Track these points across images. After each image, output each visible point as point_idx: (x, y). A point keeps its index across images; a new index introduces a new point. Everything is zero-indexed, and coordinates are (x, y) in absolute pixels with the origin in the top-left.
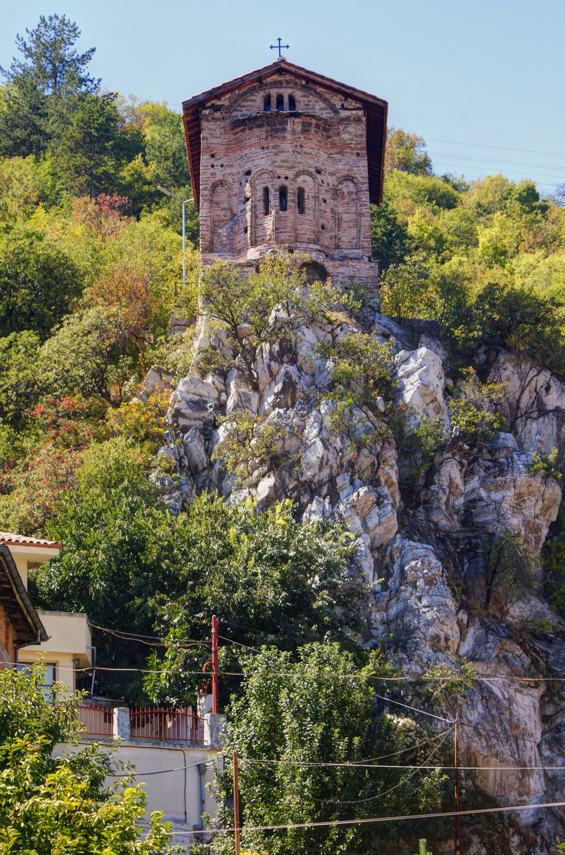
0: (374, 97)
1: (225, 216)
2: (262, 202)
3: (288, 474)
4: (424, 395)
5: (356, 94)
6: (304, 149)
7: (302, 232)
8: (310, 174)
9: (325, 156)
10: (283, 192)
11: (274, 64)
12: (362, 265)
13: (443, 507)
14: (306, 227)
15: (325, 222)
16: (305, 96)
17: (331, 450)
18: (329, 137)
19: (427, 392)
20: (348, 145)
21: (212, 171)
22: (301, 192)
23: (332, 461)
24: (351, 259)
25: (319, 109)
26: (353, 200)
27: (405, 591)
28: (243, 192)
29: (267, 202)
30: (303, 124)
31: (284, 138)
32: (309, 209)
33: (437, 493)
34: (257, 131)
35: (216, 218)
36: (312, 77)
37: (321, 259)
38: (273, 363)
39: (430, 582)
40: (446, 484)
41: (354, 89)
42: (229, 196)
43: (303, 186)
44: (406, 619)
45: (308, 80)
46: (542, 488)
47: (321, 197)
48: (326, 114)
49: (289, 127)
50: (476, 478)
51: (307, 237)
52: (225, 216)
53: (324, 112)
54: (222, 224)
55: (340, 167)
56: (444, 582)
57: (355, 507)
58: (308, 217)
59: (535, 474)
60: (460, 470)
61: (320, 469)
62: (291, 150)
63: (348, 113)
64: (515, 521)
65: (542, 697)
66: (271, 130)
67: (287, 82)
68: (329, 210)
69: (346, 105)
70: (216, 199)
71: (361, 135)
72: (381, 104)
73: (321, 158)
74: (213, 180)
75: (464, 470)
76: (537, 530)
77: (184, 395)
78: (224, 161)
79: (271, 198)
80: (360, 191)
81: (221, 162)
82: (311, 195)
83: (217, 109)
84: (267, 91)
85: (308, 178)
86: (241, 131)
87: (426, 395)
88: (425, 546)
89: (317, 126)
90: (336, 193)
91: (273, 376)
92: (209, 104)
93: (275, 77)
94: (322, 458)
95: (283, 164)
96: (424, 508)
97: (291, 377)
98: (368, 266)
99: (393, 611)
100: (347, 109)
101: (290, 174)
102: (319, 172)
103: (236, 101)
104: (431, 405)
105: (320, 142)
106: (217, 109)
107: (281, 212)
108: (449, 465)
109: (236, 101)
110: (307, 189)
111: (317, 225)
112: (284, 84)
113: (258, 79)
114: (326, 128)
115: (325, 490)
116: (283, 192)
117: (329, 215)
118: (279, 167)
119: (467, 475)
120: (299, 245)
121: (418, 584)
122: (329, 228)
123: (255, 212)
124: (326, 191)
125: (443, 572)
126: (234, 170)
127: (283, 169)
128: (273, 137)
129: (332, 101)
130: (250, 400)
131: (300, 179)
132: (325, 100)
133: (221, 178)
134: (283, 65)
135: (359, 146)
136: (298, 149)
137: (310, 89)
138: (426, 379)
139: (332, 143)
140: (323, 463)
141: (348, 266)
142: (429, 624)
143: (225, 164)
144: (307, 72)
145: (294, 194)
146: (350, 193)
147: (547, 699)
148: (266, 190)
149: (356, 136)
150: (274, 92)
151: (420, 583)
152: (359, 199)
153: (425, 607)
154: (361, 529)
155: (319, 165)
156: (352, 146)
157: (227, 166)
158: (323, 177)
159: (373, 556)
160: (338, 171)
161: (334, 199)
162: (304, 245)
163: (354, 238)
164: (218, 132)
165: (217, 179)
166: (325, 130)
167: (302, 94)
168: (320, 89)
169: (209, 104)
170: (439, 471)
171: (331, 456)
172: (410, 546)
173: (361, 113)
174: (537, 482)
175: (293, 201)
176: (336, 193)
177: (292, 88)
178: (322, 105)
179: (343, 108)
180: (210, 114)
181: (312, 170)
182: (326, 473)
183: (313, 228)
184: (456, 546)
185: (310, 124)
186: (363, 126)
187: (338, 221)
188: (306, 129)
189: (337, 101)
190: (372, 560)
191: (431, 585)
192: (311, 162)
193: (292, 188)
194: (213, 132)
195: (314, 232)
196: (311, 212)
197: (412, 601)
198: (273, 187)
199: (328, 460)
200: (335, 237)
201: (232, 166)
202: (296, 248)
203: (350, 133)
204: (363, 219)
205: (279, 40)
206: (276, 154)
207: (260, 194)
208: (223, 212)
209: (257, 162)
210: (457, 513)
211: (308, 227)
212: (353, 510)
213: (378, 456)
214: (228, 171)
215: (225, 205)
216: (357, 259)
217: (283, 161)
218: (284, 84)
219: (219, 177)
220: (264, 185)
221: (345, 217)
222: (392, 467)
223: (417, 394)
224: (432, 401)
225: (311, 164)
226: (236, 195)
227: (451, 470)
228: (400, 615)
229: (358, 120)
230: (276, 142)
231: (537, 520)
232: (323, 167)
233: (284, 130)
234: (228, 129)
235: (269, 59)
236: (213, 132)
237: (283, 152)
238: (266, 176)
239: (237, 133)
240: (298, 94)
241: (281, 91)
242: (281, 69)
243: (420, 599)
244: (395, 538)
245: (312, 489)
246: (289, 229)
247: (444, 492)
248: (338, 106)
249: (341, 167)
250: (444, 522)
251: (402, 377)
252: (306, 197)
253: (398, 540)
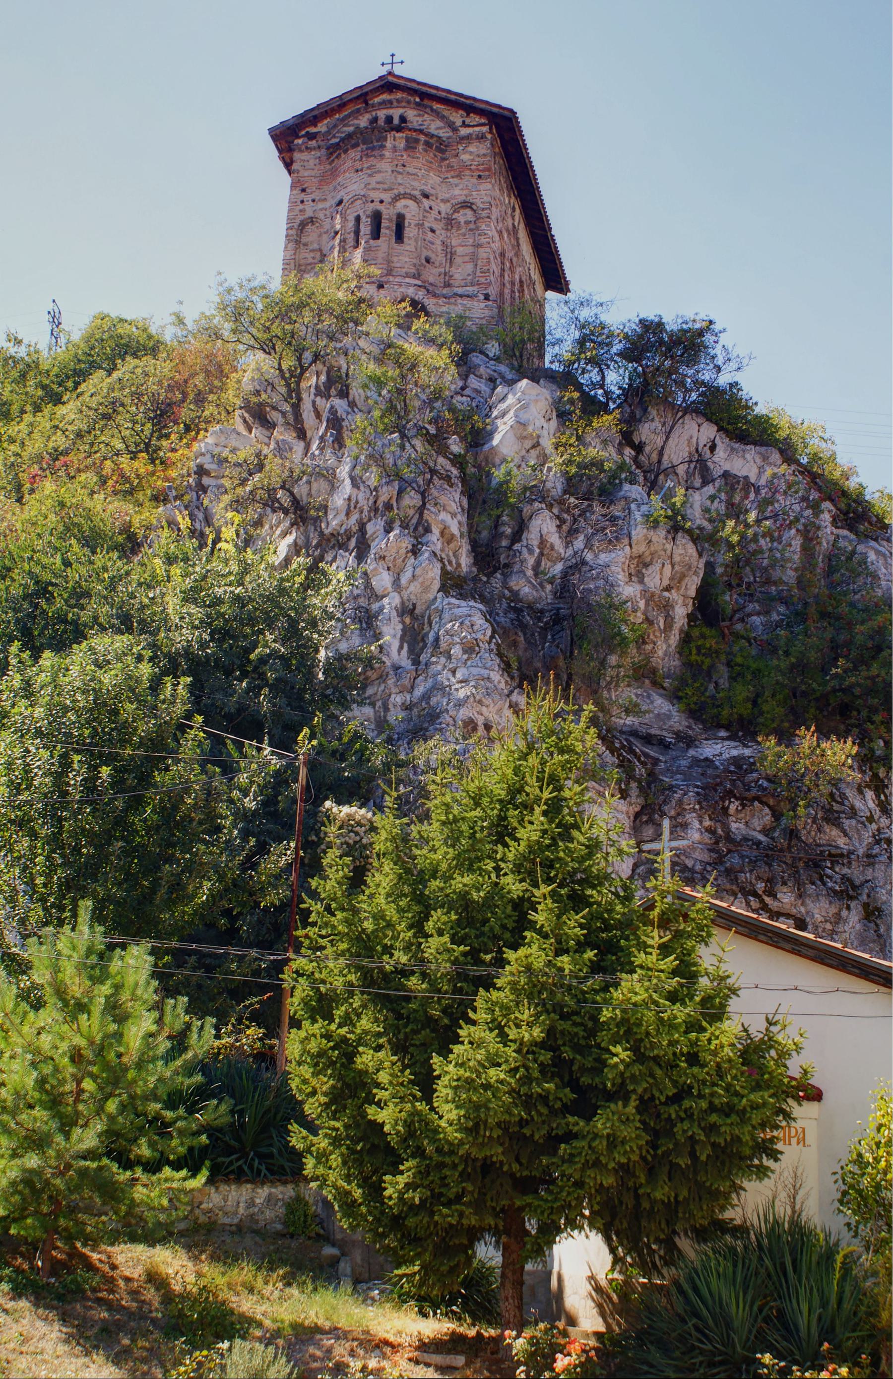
0: (499, 107)
4: (522, 438)
5: (477, 105)
8: (413, 198)
9: (438, 180)
10: (377, 218)
13: (530, 573)
20: (468, 167)
21: (301, 207)
23: (362, 502)
24: (461, 296)
25: (435, 126)
28: (333, 227)
29: (357, 232)
30: (407, 139)
31: (382, 156)
34: (352, 153)
36: (424, 89)
37: (420, 295)
38: (318, 399)
39: (470, 649)
40: (535, 543)
41: (474, 99)
42: (320, 236)
44: (434, 701)
45: (424, 95)
46: (668, 547)
47: (427, 225)
49: (389, 144)
50: (581, 537)
55: (457, 192)
57: (383, 558)
59: (655, 525)
61: (348, 514)
64: (629, 591)
65: (637, 815)
67: (398, 101)
68: (438, 242)
69: (468, 121)
70: (304, 240)
72: (506, 113)
73: (432, 181)
75: (565, 528)
76: (666, 607)
78: (316, 195)
81: (313, 196)
82: (413, 223)
83: (312, 137)
85: (410, 203)
88: (472, 603)
89: (427, 144)
90: (450, 223)
93: (385, 97)
94: (349, 499)
98: (482, 305)
99: (419, 691)
102: (427, 196)
103: (335, 126)
106: (312, 137)
108: (541, 517)
109: (335, 126)
110: (408, 216)
111: (419, 257)
113: (362, 97)
114: (440, 148)
115: (353, 543)
116: (377, 218)
117: (439, 248)
119: (570, 535)
125: (492, 637)
126: (327, 205)
128: (368, 156)
134: (390, 78)
136: (400, 168)
137: (426, 107)
138: (524, 417)
139: (449, 166)
142: (460, 704)
144: (419, 83)
145: (390, 220)
146: (467, 223)
147: (645, 818)
148: (358, 219)
150: (382, 114)
151: (456, 651)
152: (477, 228)
155: (428, 189)
159: (403, 622)
160: (454, 197)
162: (398, 279)
167: (415, 112)
168: (436, 106)
171: (361, 496)
173: (485, 129)
174: (659, 536)
175: (388, 228)
176: (450, 223)
178: (439, 123)
179: (464, 125)
182: (354, 517)
184: (540, 619)
185: (417, 141)
187: (450, 255)
188: (411, 145)
189: (457, 117)
190: (400, 626)
192: (416, 184)
193: (389, 213)
196: (412, 242)
197: (445, 677)
198: (364, 211)
202: (387, 282)
204: (481, 250)
207: (351, 224)
209: (350, 189)
210: (551, 581)
212: (381, 563)
213: (423, 494)
214: (320, 205)
215: (316, 246)
219: (309, 213)
221: (460, 250)
223: (510, 435)
224: (533, 447)
225: (416, 187)
228: (426, 697)
229: (481, 137)
231: (666, 594)
232: (433, 192)
233: (383, 147)
235: (372, 72)
241: (391, 112)
242: (389, 84)
243: (454, 672)
246: (380, 261)
247: (531, 551)
248: (459, 122)
249: (458, 193)
250: (527, 589)
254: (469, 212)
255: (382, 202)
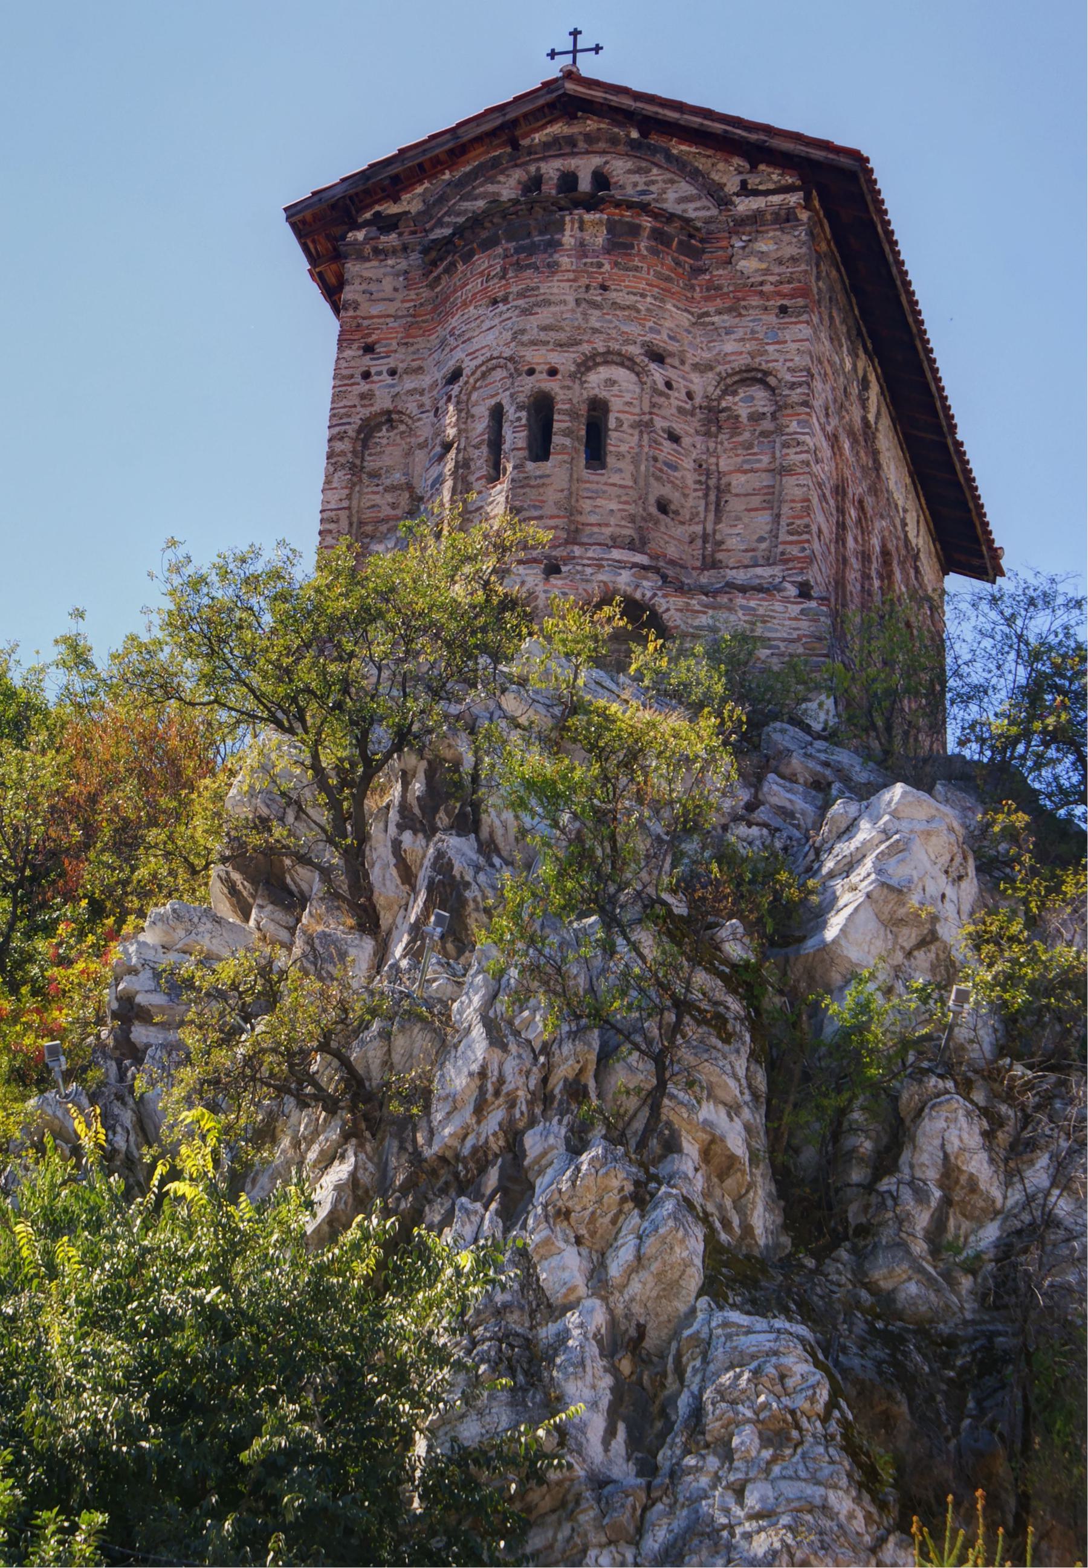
1: (394, 506)
2: (485, 449)
3: (395, 1144)
4: (893, 923)
5: (776, 143)
6: (612, 295)
7: (593, 519)
8: (627, 362)
10: (541, 409)
11: (546, 84)
12: (778, 606)
13: (919, 1247)
14: (609, 500)
15: (675, 496)
16: (638, 171)
17: (513, 1048)
18: (698, 271)
19: (901, 912)
20: (754, 288)
21: (364, 387)
22: (598, 410)
23: (513, 1082)
26: (763, 434)
27: (698, 1469)
28: (439, 432)
29: (496, 443)
30: (612, 227)
31: (553, 268)
32: (620, 456)
33: (895, 1199)
34: (482, 261)
35: (368, 515)
36: (651, 109)
37: (647, 589)
38: (407, 837)
39: (778, 1435)
41: (768, 129)
42: (409, 453)
43: (603, 394)
47: (659, 423)
48: (699, 210)
49: (568, 239)
51: (608, 531)
52: (394, 506)
53: (691, 206)
54: (384, 528)
55: (730, 347)
56: (829, 1439)
57: (565, 1214)
58: (615, 479)
60: (988, 1135)
61: (480, 1109)
62: (570, 299)
63: (757, 203)
66: (518, 251)
67: (589, 138)
68: (688, 464)
69: (753, 181)
70: (371, 464)
71: (793, 259)
74: (365, 412)
77: (150, 955)
79: (507, 432)
80: (786, 406)
81: (391, 362)
83: (388, 224)
84: (532, 169)
85: (621, 374)
86: (447, 271)
87: (901, 922)
88: (780, 1323)
89: (658, 235)
90: (714, 418)
91: (407, 875)
92: (368, 215)
94: (483, 1074)
95: (543, 336)
96: (854, 1251)
97: (450, 865)
98: (794, 609)
100: (756, 193)
101: (565, 361)
102: (658, 357)
103: (442, 199)
104: (920, 955)
105: (668, 279)
106: (388, 224)
107: (530, 466)
109: (442, 199)
110: (616, 404)
111: (643, 499)
112: (582, 145)
113: (502, 130)
114: (689, 246)
115: (493, 1178)
116: (541, 409)
117: (689, 476)
118: (533, 343)
120: (577, 551)
121: (736, 1441)
122: (686, 514)
123: (465, 480)
124: (680, 410)
126: (426, 381)
127: (543, 350)
128: (519, 267)
129: (715, 176)
130: (343, 955)
131: (596, 378)
132: (695, 175)
133: (388, 404)
134: (570, 86)
135: (786, 288)
137: (654, 150)
138: (898, 872)
139: (710, 286)
140: (487, 1089)
141: (730, 609)
143: (401, 366)
145: (573, 414)
146: (756, 417)
148: (497, 414)
149: (780, 262)
150: (551, 169)
151: (745, 1439)
153: (751, 1517)
154: (579, 1281)
155: (661, 340)
156: (767, 288)
157: (407, 371)
158: (672, 374)
159: (613, 1370)
160: (724, 358)
161: (707, 434)
163: (761, 539)
164: (388, 284)
165: (376, 408)
166: (685, 248)
167: (629, 165)
169: (368, 215)
170: (913, 1139)
171: (510, 1066)
172: (725, 1324)
173: (794, 199)
175: (567, 433)
176: (714, 418)
177: (604, 152)
178: (685, 188)
179: (745, 190)
180: (367, 239)
181: (634, 350)
182: (495, 1118)
183: (631, 509)
184: (946, 1361)
185: (635, 230)
186: (802, 233)
187: (716, 494)
188: (620, 241)
189: (727, 174)
190: (608, 1381)
191: (780, 1446)
192: (633, 329)
193: (567, 397)
194: (373, 287)
195: (632, 519)
196: (626, 466)
197: (717, 1506)
198: (510, 394)
199: (501, 1080)
200: (705, 537)
201: (419, 370)
203: (762, 256)
204: (789, 481)
205: (575, 33)
206: (526, 312)
207: (481, 426)
208: (389, 498)
210: (972, 1268)
211: (614, 506)
214: (409, 383)
215: (398, 477)
216: (760, 589)
217: (544, 329)
218: (582, 145)
219: (383, 402)
220: (493, 402)
221: (739, 482)
222: (733, 1110)
224: (923, 943)
225: (633, 335)
226: (422, 446)
227: (952, 1132)
229: (785, 219)
230: (530, 278)
232: (673, 347)
233: (554, 245)
234: (416, 274)
235: (534, 72)
236: (373, 287)
237: (548, 303)
238: (499, 374)
239: (438, 278)
240: (619, 168)
241: (572, 163)
242: (568, 100)
244: (693, 1311)
245: (451, 1178)
247: (921, 1196)
248: (732, 185)
251: (832, 875)
252: (612, 423)
253: (700, 1316)
254: (760, 394)
255: (553, 372)
